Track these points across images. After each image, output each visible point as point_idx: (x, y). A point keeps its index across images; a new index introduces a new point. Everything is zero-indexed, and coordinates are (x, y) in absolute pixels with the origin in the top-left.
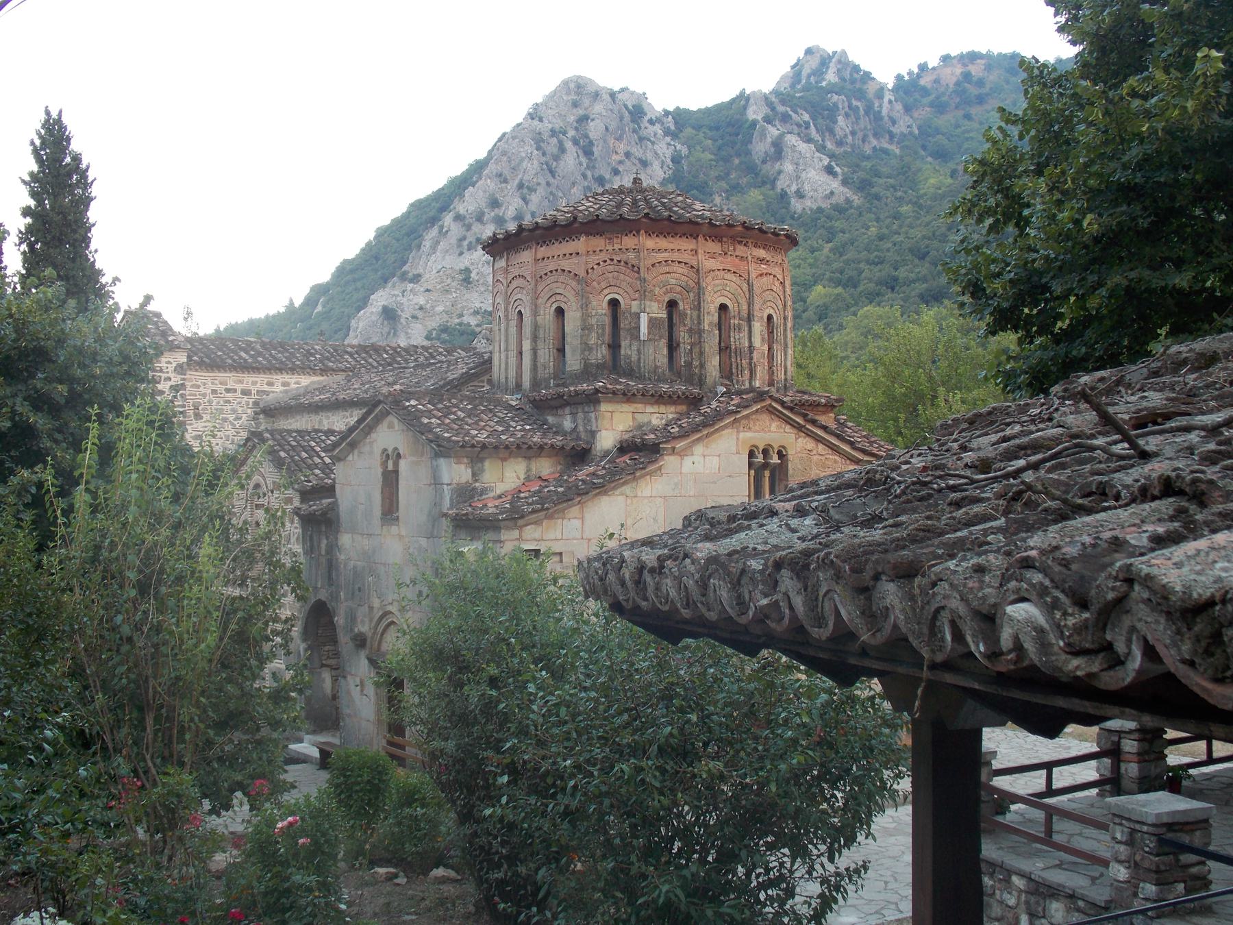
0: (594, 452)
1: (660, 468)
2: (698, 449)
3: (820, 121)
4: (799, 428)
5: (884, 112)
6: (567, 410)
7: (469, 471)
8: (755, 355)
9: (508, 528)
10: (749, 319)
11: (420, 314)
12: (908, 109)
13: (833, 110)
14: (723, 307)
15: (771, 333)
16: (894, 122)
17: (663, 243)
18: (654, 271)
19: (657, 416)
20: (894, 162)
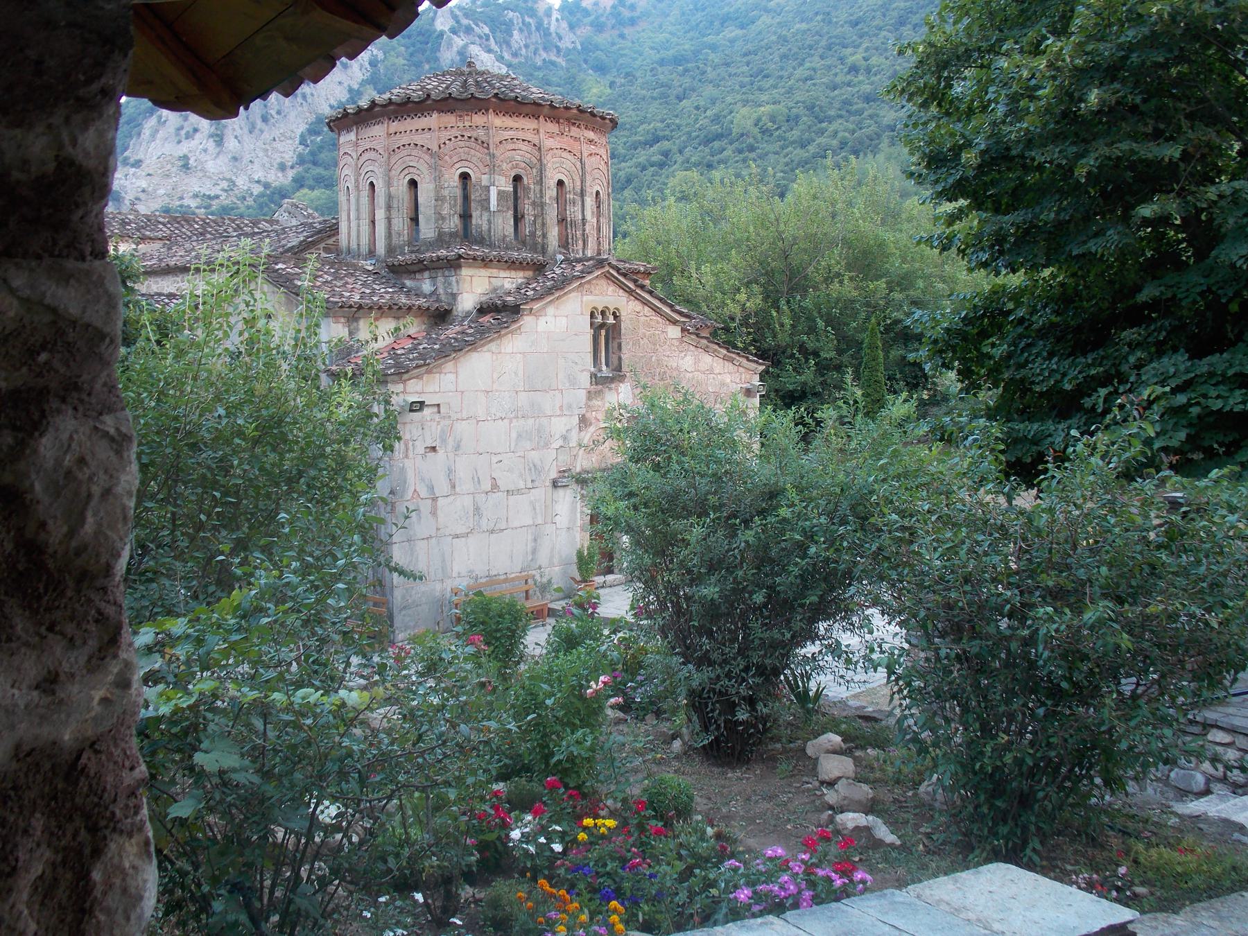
0: (455, 313)
1: (519, 328)
2: (551, 310)
3: (498, 34)
4: (630, 292)
5: (552, 29)
6: (426, 274)
7: (346, 330)
8: (588, 227)
9: (394, 382)
10: (582, 194)
11: (142, 196)
12: (572, 27)
13: (508, 27)
14: (560, 183)
15: (598, 207)
16: (560, 38)
17: (508, 121)
18: (502, 148)
19: (509, 281)
20: (561, 73)
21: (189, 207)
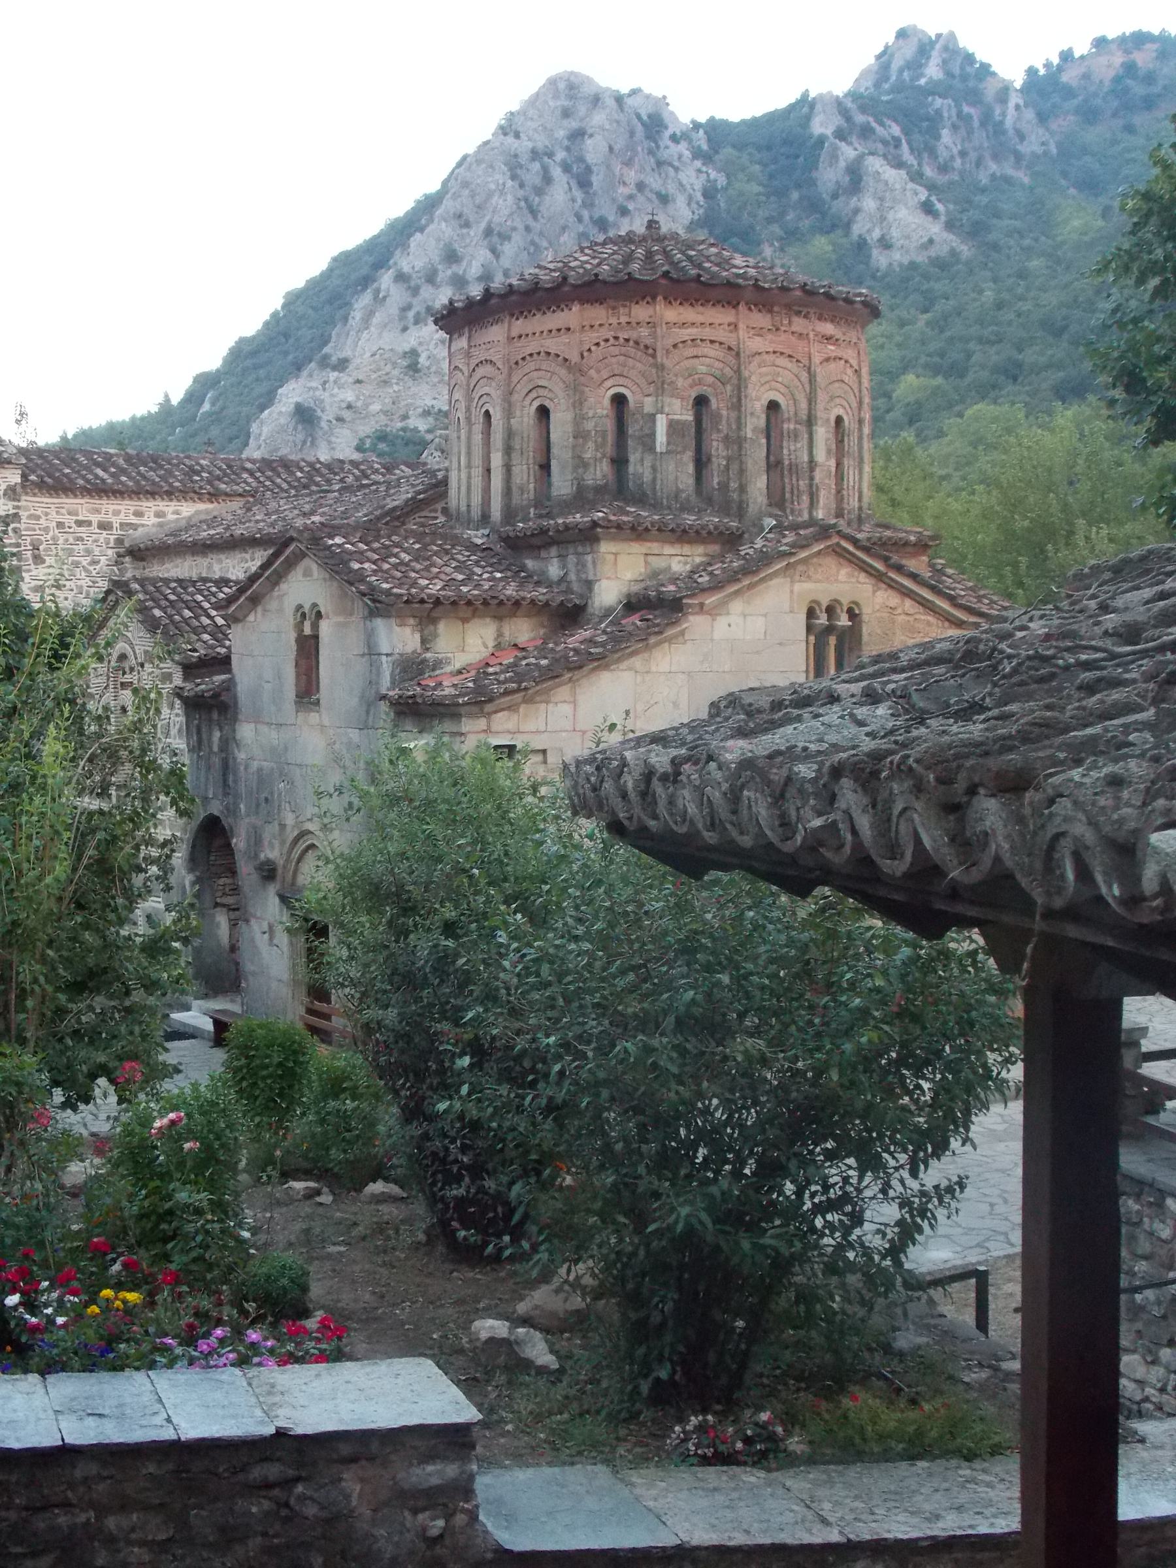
0: (590, 610)
1: (682, 633)
2: (737, 606)
3: (916, 137)
4: (879, 577)
5: (1009, 122)
6: (554, 551)
7: (417, 636)
8: (818, 475)
9: (470, 715)
11: (347, 415)
13: (933, 124)
14: (773, 406)
17: (689, 314)
21: (416, 430)
